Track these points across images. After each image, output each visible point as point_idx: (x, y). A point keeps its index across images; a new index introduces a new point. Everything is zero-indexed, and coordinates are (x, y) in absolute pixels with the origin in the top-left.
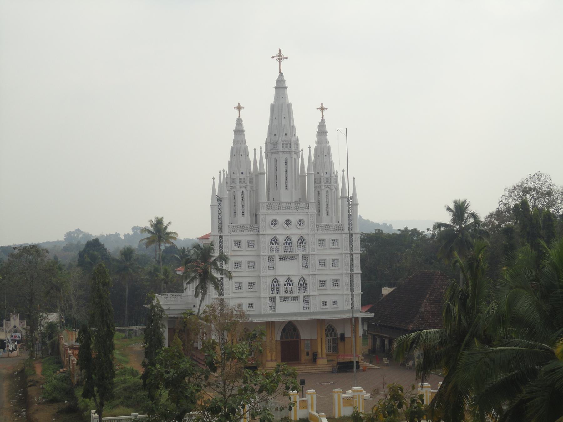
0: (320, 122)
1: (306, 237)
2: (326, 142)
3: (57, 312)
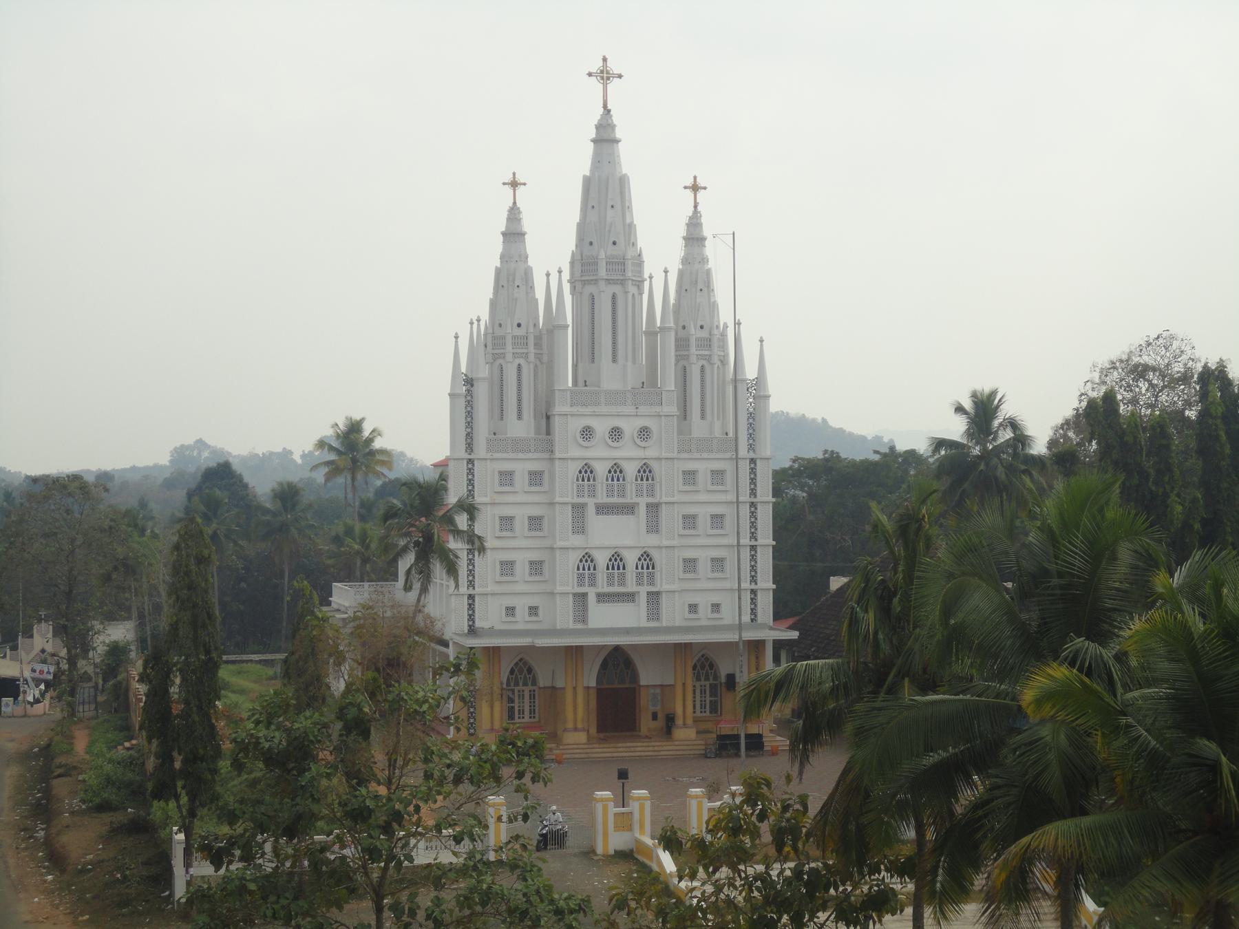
0: (690, 217)
1: (654, 465)
2: (703, 259)
3: (129, 618)
